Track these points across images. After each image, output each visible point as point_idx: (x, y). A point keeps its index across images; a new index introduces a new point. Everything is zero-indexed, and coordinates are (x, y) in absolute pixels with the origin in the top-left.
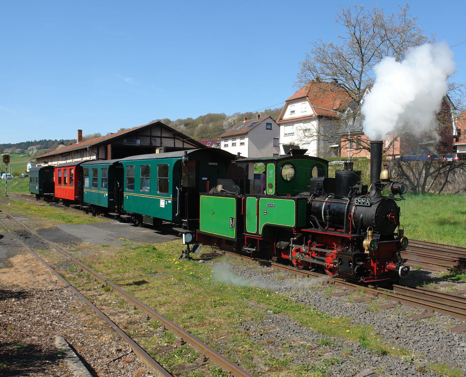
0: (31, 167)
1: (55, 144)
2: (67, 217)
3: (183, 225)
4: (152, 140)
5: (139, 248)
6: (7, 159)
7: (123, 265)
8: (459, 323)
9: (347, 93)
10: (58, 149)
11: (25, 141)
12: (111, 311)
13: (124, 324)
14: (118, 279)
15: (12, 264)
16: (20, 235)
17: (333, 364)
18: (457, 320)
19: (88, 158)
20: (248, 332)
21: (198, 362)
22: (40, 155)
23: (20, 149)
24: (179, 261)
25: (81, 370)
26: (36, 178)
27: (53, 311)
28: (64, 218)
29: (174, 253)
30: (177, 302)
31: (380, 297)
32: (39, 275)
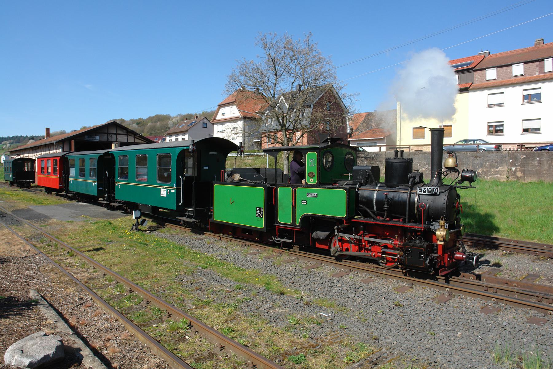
0: (4, 159)
1: (26, 139)
3: (187, 213)
5: (98, 223)
7: (84, 236)
8: (339, 271)
9: (264, 100)
10: (28, 143)
12: (74, 271)
13: (85, 280)
17: (243, 302)
18: (337, 269)
20: (182, 282)
21: (142, 304)
22: (12, 149)
24: (130, 232)
25: (51, 313)
26: (10, 168)
27: (27, 272)
28: (34, 201)
29: (126, 227)
30: (127, 262)
31: (283, 255)
32: (14, 246)
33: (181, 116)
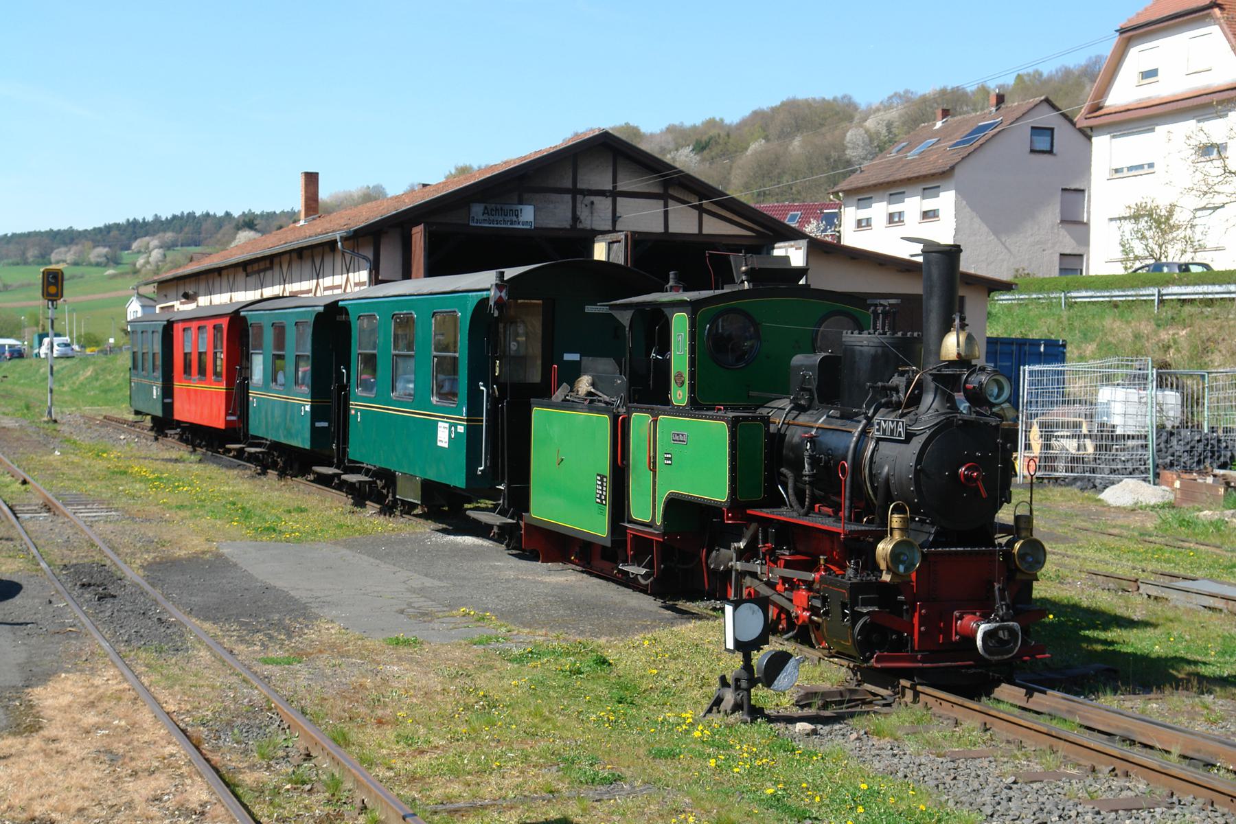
0: (139, 315)
2: (258, 512)
4: (579, 205)
5: (540, 655)
6: (53, 284)
11: (122, 220)
14: (457, 805)
15: (37, 716)
16: (83, 585)
19: (276, 290)
22: (171, 269)
23: (105, 246)
26: (154, 354)
28: (246, 514)
29: (682, 685)
32: (134, 774)
33: (908, 100)
